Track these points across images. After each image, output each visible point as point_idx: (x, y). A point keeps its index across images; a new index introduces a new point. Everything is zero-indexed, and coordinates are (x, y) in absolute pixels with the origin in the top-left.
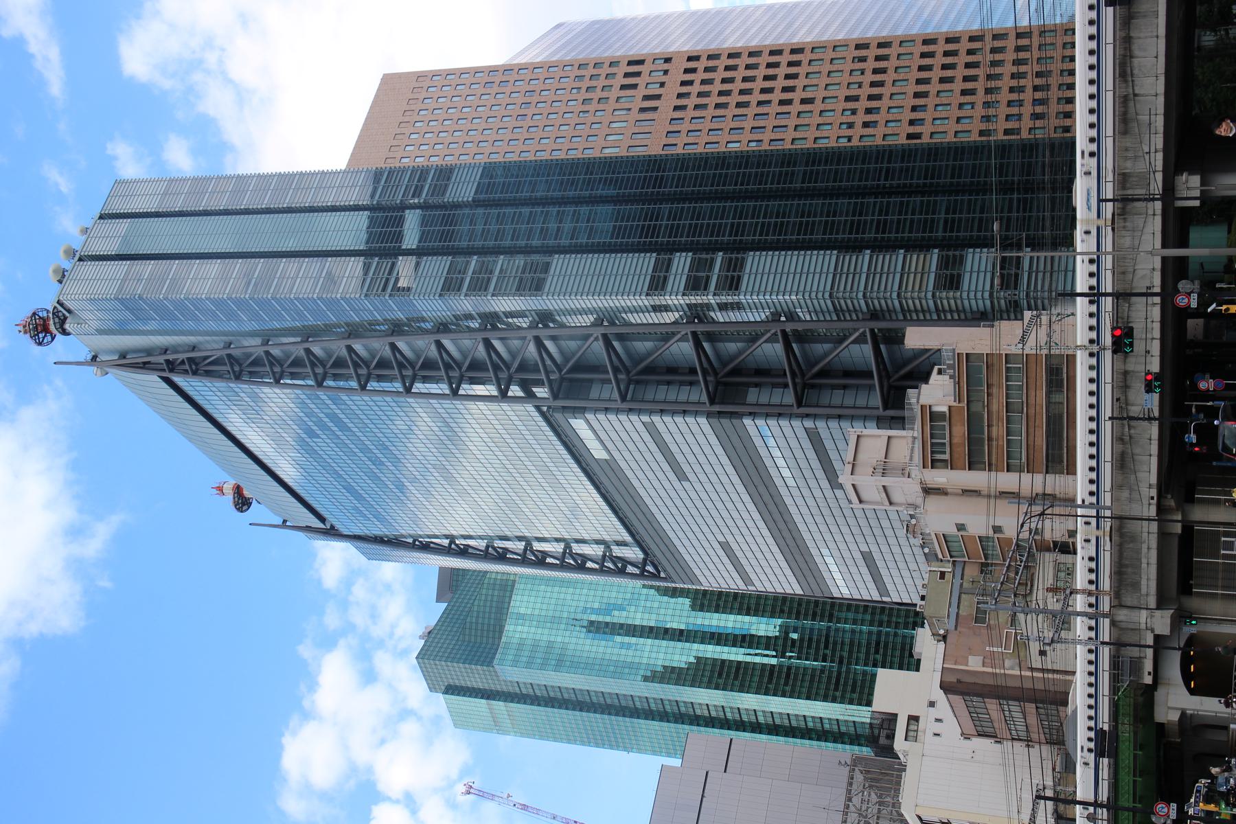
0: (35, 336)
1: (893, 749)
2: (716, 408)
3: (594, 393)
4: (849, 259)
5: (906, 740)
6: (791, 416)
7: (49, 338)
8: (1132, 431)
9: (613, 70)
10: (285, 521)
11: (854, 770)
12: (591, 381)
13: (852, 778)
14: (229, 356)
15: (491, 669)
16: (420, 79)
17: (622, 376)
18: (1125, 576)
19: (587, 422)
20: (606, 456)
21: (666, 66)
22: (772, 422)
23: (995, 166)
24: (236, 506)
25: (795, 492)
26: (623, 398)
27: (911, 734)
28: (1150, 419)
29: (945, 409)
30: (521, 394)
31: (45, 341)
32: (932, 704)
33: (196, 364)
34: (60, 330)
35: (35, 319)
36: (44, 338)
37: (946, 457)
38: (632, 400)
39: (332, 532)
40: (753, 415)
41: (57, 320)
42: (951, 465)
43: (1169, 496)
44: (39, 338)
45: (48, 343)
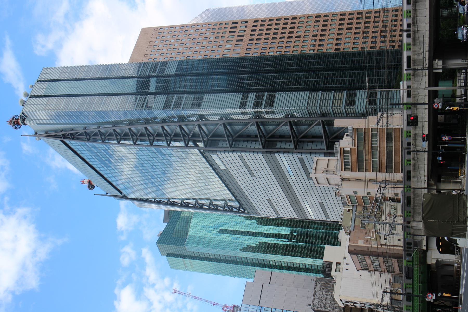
0: (14, 125)
1: (331, 275)
2: (265, 150)
3: (220, 145)
4: (314, 95)
5: (336, 271)
6: (293, 153)
7: (19, 126)
8: (418, 156)
9: (226, 26)
10: (107, 193)
11: (317, 283)
12: (219, 140)
13: (316, 286)
14: (85, 132)
15: (184, 247)
16: (155, 30)
17: (230, 139)
18: (416, 210)
19: (218, 155)
20: (225, 168)
21: (246, 24)
22: (286, 155)
23: (329, 284)
24: (89, 188)
25: (295, 181)
26: (231, 147)
27: (338, 269)
28: (424, 151)
29: (349, 149)
30: (193, 145)
31: (18, 127)
32: (345, 258)
33: (73, 136)
34: (23, 123)
35: (14, 119)
36: (17, 126)
37: (350, 167)
38: (234, 147)
39: (124, 197)
40: (279, 152)
41: (22, 120)
42: (352, 170)
43: (432, 180)
44: (15, 126)
45: (19, 128)
